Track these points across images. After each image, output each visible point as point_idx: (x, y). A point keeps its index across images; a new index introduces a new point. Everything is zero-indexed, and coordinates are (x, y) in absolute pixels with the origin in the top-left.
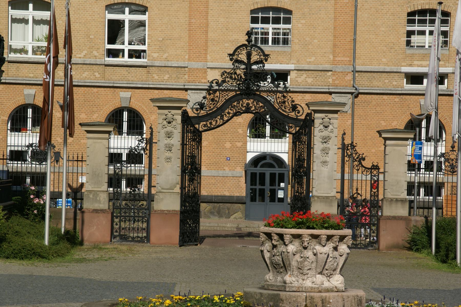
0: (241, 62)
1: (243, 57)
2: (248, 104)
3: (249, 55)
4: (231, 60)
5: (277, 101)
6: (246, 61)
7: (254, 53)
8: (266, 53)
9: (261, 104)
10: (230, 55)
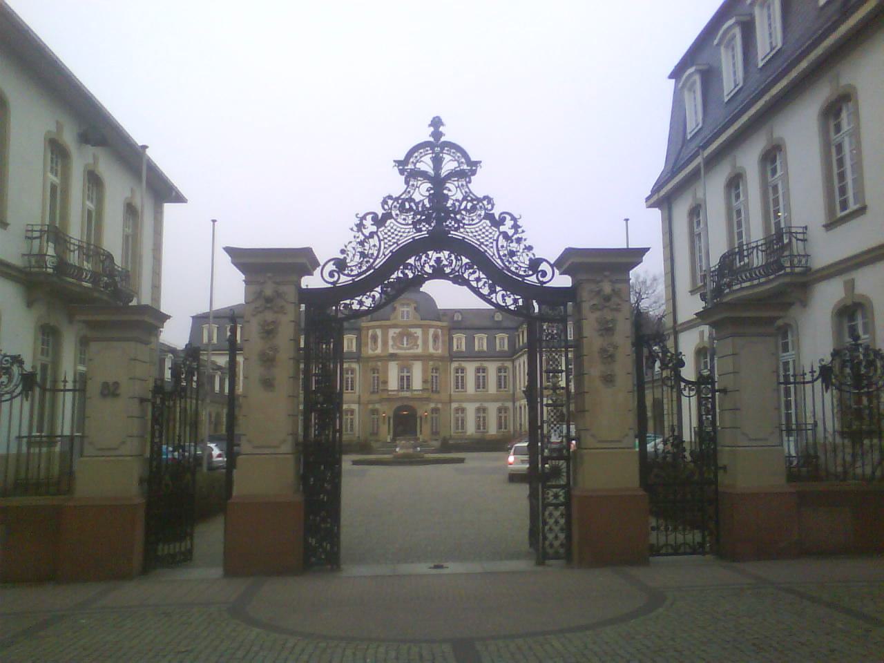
0: (424, 175)
1: (426, 164)
2: (438, 260)
3: (437, 162)
4: (402, 172)
5: (499, 254)
6: (431, 172)
7: (447, 158)
8: (473, 159)
9: (465, 260)
10: (399, 163)
